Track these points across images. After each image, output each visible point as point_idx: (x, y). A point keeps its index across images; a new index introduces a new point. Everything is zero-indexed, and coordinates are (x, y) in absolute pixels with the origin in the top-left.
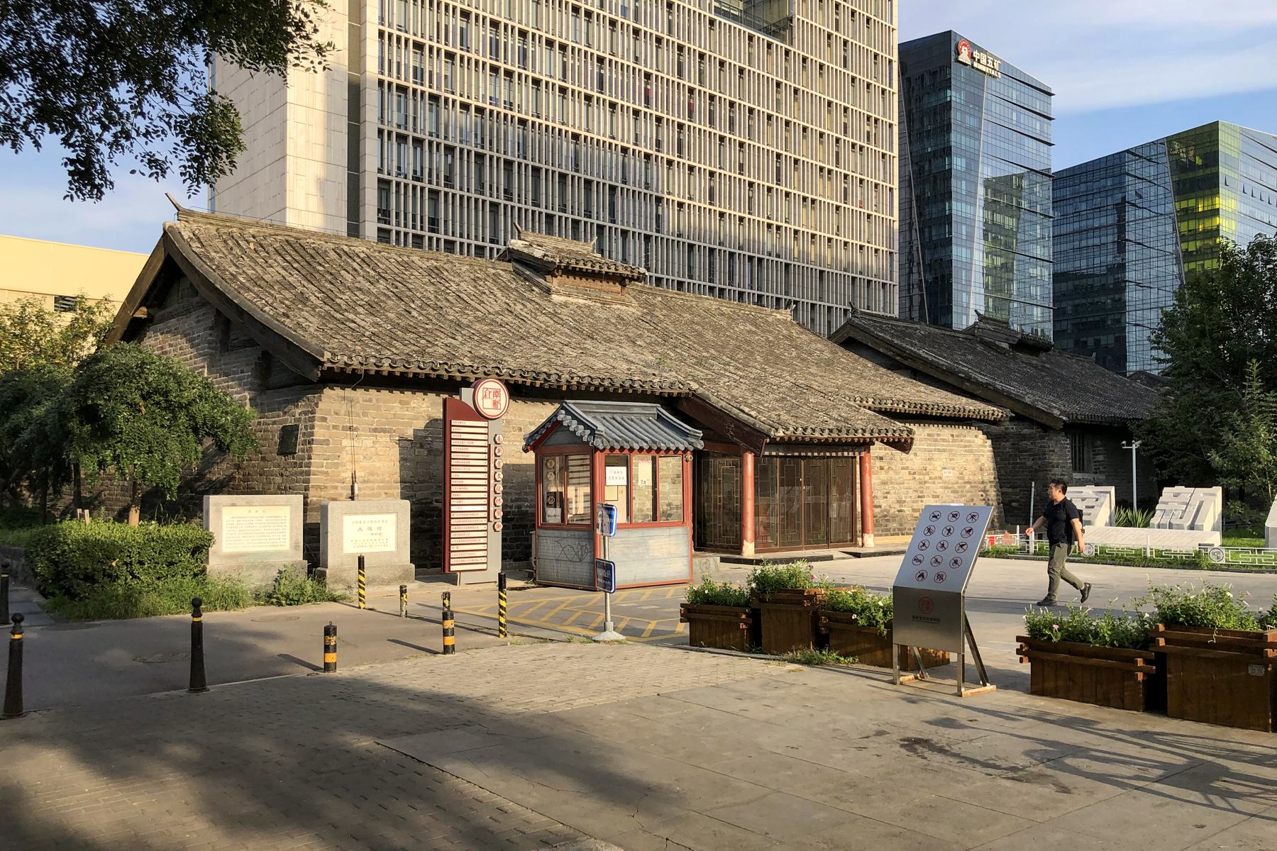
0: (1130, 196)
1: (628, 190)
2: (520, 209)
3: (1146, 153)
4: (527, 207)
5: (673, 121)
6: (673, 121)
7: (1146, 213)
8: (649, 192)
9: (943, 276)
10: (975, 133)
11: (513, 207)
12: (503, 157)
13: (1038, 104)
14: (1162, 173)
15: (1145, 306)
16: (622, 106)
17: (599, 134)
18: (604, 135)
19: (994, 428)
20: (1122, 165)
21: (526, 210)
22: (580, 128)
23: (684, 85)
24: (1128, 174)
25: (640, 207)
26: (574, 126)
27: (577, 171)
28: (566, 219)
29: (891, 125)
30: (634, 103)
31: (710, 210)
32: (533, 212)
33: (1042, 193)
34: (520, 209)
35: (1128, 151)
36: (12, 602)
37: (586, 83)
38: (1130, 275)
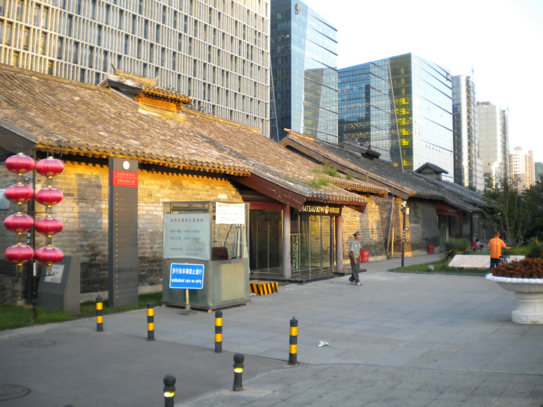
0: (372, 84)
1: (128, 58)
2: (66, 65)
3: (380, 64)
4: (70, 63)
5: (154, 23)
6: (130, 13)
7: (380, 94)
8: (99, 47)
9: (286, 117)
10: (303, 47)
11: (62, 63)
12: (58, 34)
13: (331, 33)
14: (385, 73)
15: (380, 138)
16: (127, 12)
17: (113, 25)
18: (116, 27)
19: (380, 200)
20: (369, 68)
21: (70, 65)
22: (102, 22)
23: (161, 4)
24: (372, 74)
25: (196, 88)
26: (99, 20)
27: (70, 36)
28: (92, 72)
29: (266, 37)
30: (157, 20)
31: (138, 61)
32: (74, 67)
33: (333, 80)
34: (66, 65)
35: (372, 63)
36: (120, 271)
37: (151, 16)
38: (373, 123)
